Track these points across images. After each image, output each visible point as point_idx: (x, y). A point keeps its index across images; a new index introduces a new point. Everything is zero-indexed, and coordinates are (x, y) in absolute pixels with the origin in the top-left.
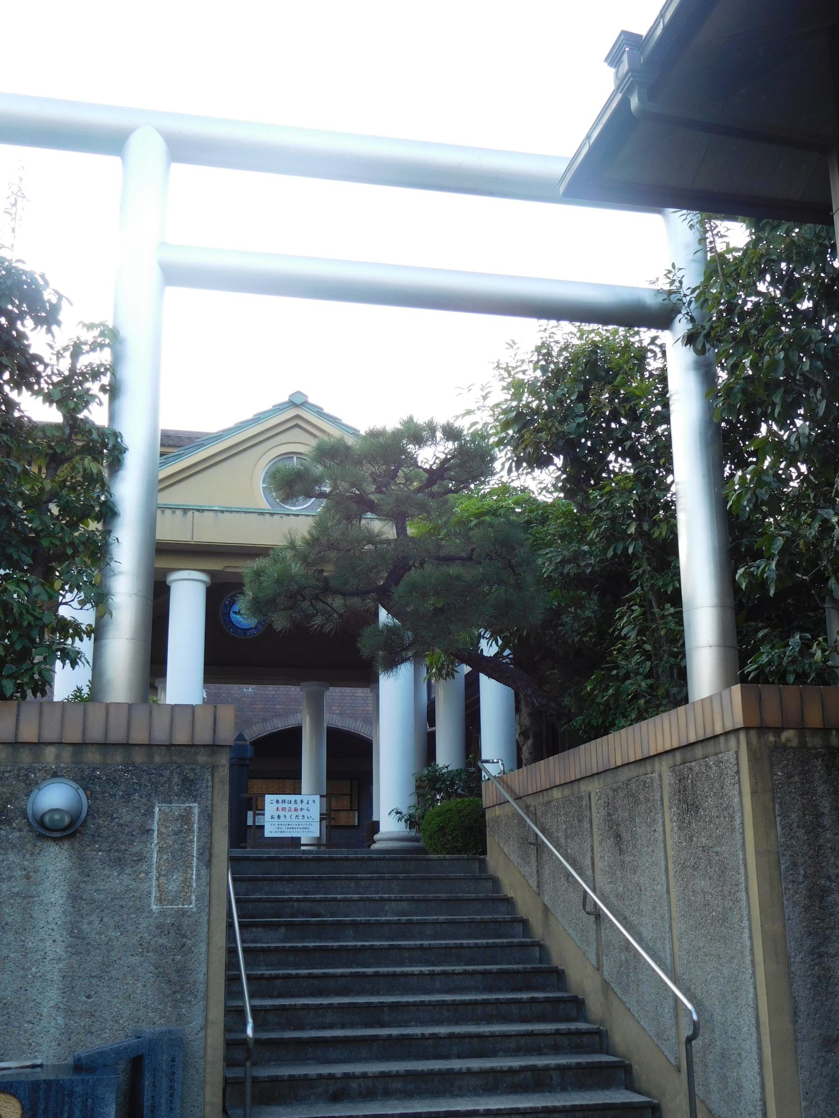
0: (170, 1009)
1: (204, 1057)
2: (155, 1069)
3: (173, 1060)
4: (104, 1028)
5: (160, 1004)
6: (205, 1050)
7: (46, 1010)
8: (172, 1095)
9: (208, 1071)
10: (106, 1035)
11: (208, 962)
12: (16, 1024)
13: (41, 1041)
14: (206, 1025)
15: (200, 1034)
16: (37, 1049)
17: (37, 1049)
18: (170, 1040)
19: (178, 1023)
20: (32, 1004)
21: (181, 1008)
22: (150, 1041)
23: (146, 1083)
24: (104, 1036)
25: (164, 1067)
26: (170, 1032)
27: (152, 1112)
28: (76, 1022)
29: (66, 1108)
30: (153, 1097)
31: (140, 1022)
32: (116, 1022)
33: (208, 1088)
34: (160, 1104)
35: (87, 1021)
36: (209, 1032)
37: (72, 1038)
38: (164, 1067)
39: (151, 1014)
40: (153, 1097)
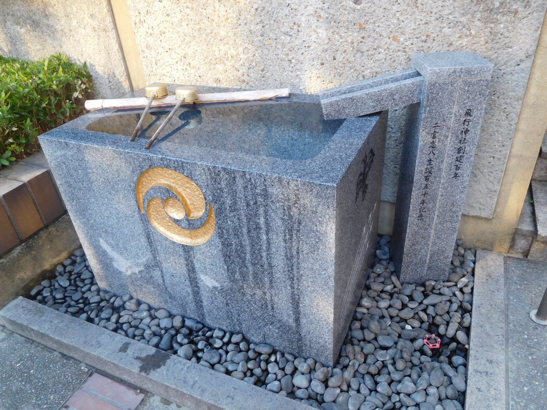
0: (478, 23)
1: (522, 99)
2: (436, 126)
3: (468, 113)
4: (378, 47)
5: (463, 15)
6: (527, 88)
7: (303, 19)
8: (459, 160)
9: (523, 116)
10: (381, 56)
11: (10, 220)
12: (271, 35)
13: (302, 58)
14: (536, 52)
15: (522, 65)
16: (298, 66)
17: (298, 66)
18: (466, 83)
19: (489, 45)
20: (286, 10)
21: (496, 22)
22: (433, 85)
23: (421, 143)
24: (377, 57)
25: (452, 122)
26: (469, 72)
27: (427, 179)
28: (341, 37)
29: (261, 211)
30: (430, 160)
31: (430, 40)
32: (395, 39)
33: (520, 136)
34: (440, 169)
35: (355, 36)
36: (539, 61)
37: (337, 57)
38: (452, 122)
39: (447, 31)
40: (430, 160)
